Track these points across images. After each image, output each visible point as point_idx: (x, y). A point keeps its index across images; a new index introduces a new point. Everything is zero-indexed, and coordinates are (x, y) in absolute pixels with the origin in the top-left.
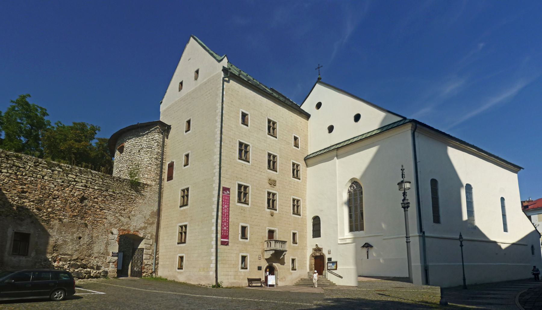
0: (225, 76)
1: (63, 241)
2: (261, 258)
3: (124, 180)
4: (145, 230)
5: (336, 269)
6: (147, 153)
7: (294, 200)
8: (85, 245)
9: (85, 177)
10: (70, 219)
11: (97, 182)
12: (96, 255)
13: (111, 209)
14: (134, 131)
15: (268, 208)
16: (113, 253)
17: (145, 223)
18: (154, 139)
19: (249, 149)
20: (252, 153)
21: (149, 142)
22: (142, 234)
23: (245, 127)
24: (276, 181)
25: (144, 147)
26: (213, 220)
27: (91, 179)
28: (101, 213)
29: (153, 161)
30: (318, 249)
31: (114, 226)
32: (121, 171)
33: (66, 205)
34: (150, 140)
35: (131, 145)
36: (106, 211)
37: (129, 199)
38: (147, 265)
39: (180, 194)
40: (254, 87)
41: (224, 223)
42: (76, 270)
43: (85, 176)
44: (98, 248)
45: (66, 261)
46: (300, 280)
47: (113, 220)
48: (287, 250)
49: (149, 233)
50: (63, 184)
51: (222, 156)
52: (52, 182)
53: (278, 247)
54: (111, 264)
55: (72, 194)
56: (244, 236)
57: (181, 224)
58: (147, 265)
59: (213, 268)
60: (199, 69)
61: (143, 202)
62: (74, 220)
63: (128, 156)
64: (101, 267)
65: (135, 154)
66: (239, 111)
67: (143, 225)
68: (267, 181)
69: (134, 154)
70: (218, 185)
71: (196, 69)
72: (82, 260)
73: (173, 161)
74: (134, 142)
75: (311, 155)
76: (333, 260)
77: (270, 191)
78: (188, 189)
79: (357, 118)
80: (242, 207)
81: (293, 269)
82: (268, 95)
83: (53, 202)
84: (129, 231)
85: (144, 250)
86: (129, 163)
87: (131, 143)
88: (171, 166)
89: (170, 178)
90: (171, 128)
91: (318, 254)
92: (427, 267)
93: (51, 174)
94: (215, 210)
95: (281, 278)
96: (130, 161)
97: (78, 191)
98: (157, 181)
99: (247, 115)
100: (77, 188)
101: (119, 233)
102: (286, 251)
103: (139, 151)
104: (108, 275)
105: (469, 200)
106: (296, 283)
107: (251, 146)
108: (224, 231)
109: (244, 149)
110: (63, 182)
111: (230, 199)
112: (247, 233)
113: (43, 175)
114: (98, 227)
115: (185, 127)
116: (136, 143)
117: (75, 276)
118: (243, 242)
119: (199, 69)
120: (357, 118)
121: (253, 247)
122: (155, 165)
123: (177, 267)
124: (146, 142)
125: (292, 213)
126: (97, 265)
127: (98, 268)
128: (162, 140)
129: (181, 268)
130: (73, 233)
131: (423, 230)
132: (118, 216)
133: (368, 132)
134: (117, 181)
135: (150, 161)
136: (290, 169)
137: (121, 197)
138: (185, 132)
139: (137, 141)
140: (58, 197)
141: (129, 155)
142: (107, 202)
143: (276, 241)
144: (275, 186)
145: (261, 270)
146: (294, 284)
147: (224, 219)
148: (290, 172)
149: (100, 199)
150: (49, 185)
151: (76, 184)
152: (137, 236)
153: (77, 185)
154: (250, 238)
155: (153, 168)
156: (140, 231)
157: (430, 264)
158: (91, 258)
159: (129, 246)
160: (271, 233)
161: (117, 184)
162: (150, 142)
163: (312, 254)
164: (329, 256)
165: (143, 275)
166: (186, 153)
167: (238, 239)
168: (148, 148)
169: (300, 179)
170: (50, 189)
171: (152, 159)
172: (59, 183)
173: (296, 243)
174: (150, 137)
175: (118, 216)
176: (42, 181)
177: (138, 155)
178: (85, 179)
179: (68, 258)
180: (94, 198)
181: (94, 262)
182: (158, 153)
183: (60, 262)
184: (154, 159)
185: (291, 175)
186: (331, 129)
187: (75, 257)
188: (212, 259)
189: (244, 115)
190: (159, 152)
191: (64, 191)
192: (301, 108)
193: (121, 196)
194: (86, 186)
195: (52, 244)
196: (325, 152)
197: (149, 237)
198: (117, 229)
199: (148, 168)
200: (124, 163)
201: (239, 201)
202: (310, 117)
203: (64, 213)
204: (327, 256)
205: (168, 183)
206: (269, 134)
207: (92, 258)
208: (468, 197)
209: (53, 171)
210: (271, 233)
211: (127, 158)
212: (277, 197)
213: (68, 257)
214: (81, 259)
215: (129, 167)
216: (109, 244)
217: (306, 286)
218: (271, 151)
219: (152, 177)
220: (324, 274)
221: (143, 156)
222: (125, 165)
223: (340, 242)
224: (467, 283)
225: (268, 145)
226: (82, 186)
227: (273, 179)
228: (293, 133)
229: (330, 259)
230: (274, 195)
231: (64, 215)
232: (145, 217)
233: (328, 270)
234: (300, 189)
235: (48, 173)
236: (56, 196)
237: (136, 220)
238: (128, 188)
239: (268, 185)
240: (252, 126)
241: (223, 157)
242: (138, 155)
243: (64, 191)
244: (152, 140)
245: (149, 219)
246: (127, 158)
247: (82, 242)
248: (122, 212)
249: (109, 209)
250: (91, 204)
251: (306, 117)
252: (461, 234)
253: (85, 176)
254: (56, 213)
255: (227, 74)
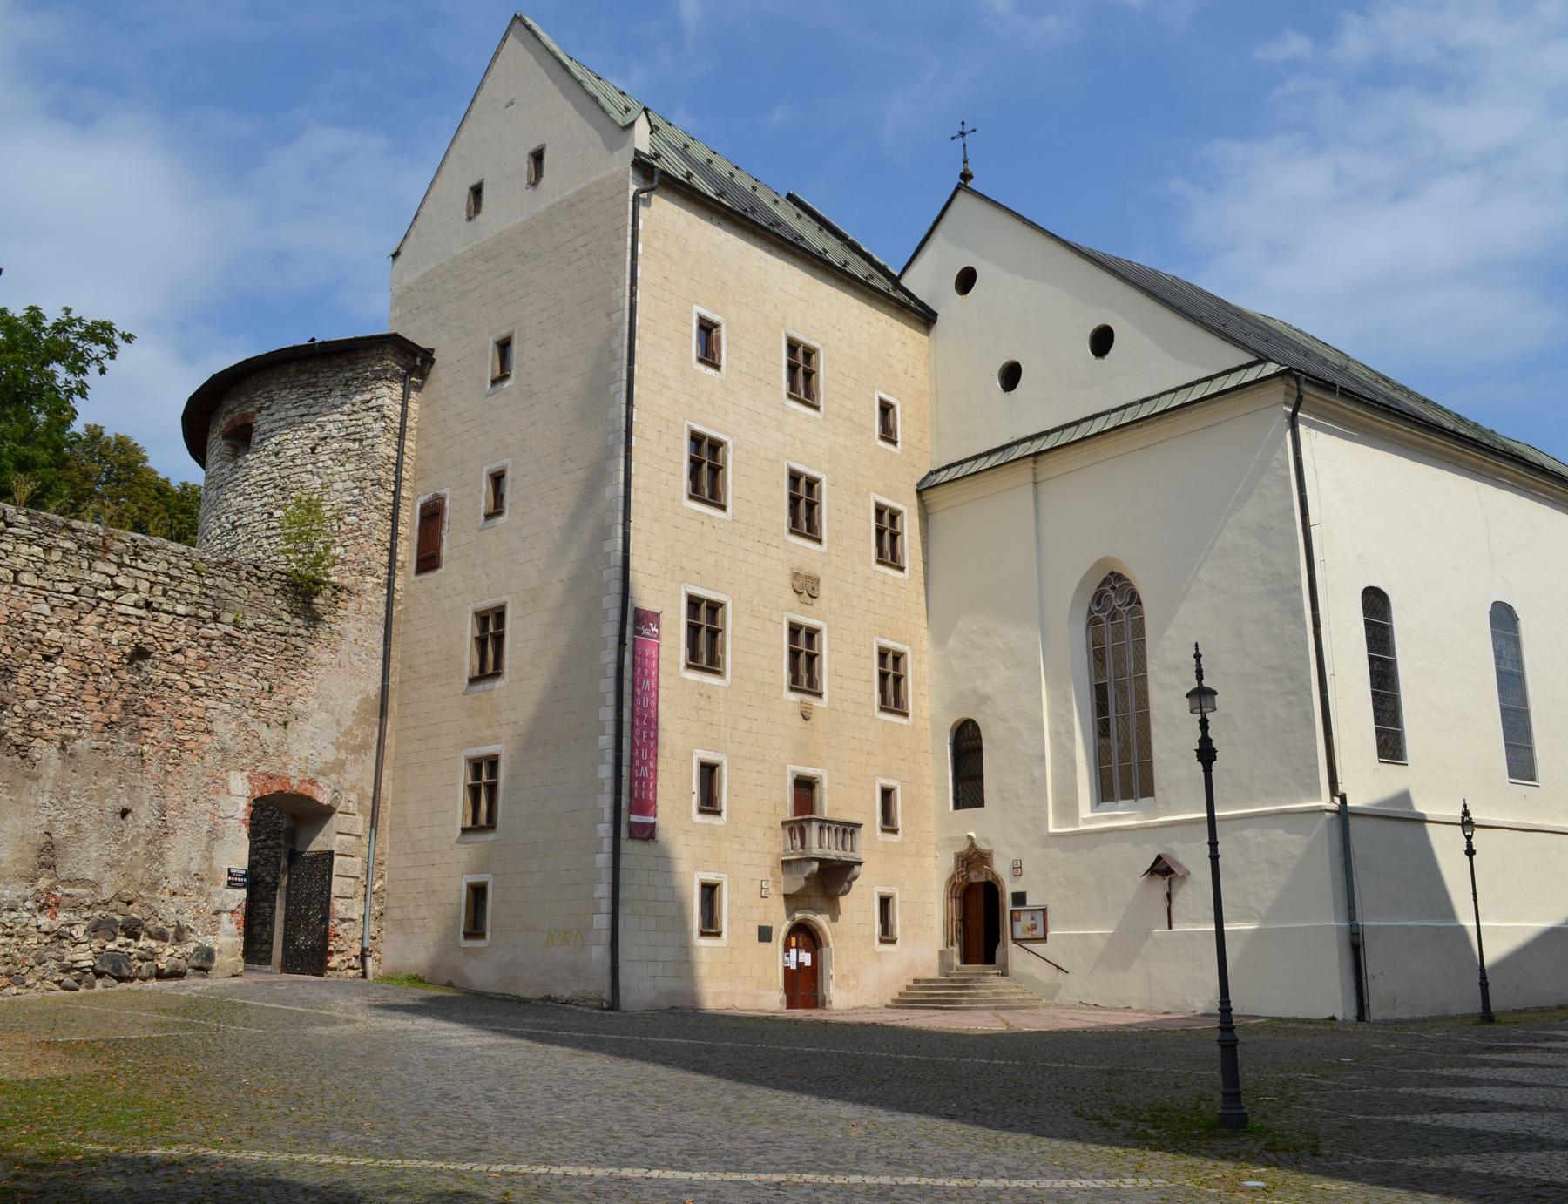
0: (643, 187)
1: (70, 828)
2: (771, 890)
3: (272, 575)
4: (339, 773)
5: (1044, 939)
6: (342, 458)
7: (883, 654)
8: (141, 842)
9: (145, 571)
10: (95, 737)
11: (184, 585)
12: (176, 882)
13: (225, 691)
14: (293, 369)
15: (792, 689)
16: (230, 874)
17: (338, 746)
18: (370, 405)
19: (725, 458)
20: (733, 472)
21: (352, 417)
22: (329, 790)
23: (711, 371)
24: (817, 581)
25: (334, 433)
26: (601, 738)
27: (167, 575)
28: (193, 710)
29: (367, 491)
30: (973, 858)
31: (236, 763)
32: (240, 526)
33: (84, 682)
34: (355, 409)
35: (282, 423)
36: (212, 703)
37: (286, 649)
38: (343, 920)
39: (470, 630)
40: (739, 219)
41: (640, 752)
42: (111, 946)
43: (144, 566)
44: (182, 854)
45: (75, 909)
46: (911, 983)
47: (234, 736)
48: (863, 859)
49: (353, 788)
50: (76, 599)
51: (632, 490)
52: (45, 593)
53: (832, 850)
54: (225, 917)
55: (104, 639)
56: (709, 802)
57: (474, 752)
58: (343, 920)
59: (602, 932)
60: (545, 145)
61: (333, 662)
62: (108, 744)
63: (267, 468)
64: (192, 931)
65: (298, 462)
66: (690, 313)
67: (330, 755)
68: (786, 581)
69: (293, 461)
70: (618, 602)
71: (533, 146)
72: (129, 903)
73: (442, 492)
74: (293, 412)
75: (942, 474)
76: (1031, 901)
77: (801, 619)
78: (499, 614)
79: (1102, 341)
80: (703, 685)
81: (885, 938)
82: (787, 245)
83: (45, 674)
84: (286, 780)
85: (337, 859)
86: (272, 496)
87: (283, 415)
88: (432, 515)
89: (428, 561)
90: (432, 361)
91: (975, 877)
92: (1358, 934)
93: (39, 565)
94: (611, 699)
95: (843, 976)
96: (277, 490)
97: (125, 624)
98: (379, 573)
99: (716, 326)
100: (121, 614)
101: (253, 791)
102: (860, 863)
103: (313, 450)
104: (215, 965)
105: (1509, 668)
106: (896, 997)
107: (730, 445)
108: (640, 784)
109: (706, 459)
110: (76, 592)
111: (662, 656)
112: (720, 792)
113: (18, 567)
114: (184, 766)
115: (490, 367)
116: (302, 416)
117: (106, 969)
118: (704, 825)
119: (545, 145)
120: (1102, 341)
121: (739, 847)
122: (376, 507)
123: (462, 930)
124: (342, 413)
125: (876, 708)
126: (178, 922)
127: (180, 935)
128: (399, 408)
129: (478, 931)
130: (103, 793)
131: (1341, 789)
132: (249, 719)
133: (1141, 398)
134: (247, 579)
135: (356, 492)
136: (869, 531)
137: (260, 643)
138: (490, 382)
139: (304, 411)
140: (58, 654)
141: (271, 464)
142: (214, 666)
143: (824, 824)
144: (814, 600)
145: (770, 940)
146: (890, 1003)
147: (641, 735)
148: (870, 543)
149: (191, 654)
150: (34, 609)
151: (118, 597)
152: (310, 799)
153: (119, 600)
154: (728, 809)
155: (367, 522)
156: (321, 778)
157: (1367, 922)
158: (157, 895)
159: (270, 843)
160: (805, 787)
161: (249, 592)
162: (356, 416)
163: (954, 876)
164: (1018, 888)
165: (329, 965)
166: (495, 466)
167: (689, 816)
168: (347, 437)
169: (902, 569)
170: (36, 621)
171: (363, 484)
172: (65, 596)
173: (895, 831)
174: (358, 398)
175: (249, 719)
176: (13, 592)
177: (310, 467)
178: (145, 575)
179: (86, 896)
180: (176, 651)
181: (169, 911)
182: (386, 462)
183: (60, 914)
184: (373, 485)
185: (870, 555)
186: (1011, 376)
187: (107, 893)
188: (598, 894)
189: (707, 329)
190: (389, 457)
191: (78, 627)
192: (904, 282)
193: (259, 639)
194: (148, 605)
195: (34, 842)
196: (991, 468)
197: (350, 804)
198: (246, 773)
199: (348, 519)
200: (253, 495)
201: (693, 662)
202: (935, 322)
203: (76, 714)
204: (1009, 888)
205: (420, 581)
206: (790, 397)
207: (162, 897)
208: (1504, 653)
209: (48, 549)
210: (805, 787)
211: (265, 477)
212: (825, 646)
213: (83, 891)
214: (128, 898)
215: (271, 514)
216: (217, 838)
217: (936, 1008)
218: (801, 463)
219: (362, 555)
220: (998, 958)
221: (329, 471)
222: (257, 503)
223: (1056, 826)
224: (1496, 1003)
225: (788, 438)
226: (136, 606)
227: (806, 570)
228: (874, 388)
229: (1019, 898)
230: (812, 634)
231: (77, 723)
232: (338, 722)
233: (1016, 941)
234: (903, 607)
235: (32, 558)
236: (52, 648)
237: (308, 735)
238: (284, 606)
239: (791, 595)
240: (733, 368)
241: (635, 493)
242: (310, 467)
243: (78, 627)
244: (363, 407)
245: (351, 728)
246: (265, 477)
247: (130, 828)
248: (264, 702)
249: (222, 694)
250: (162, 674)
251: (920, 321)
252: (1465, 806)
253: (144, 566)
254: (52, 718)
255: (652, 180)
